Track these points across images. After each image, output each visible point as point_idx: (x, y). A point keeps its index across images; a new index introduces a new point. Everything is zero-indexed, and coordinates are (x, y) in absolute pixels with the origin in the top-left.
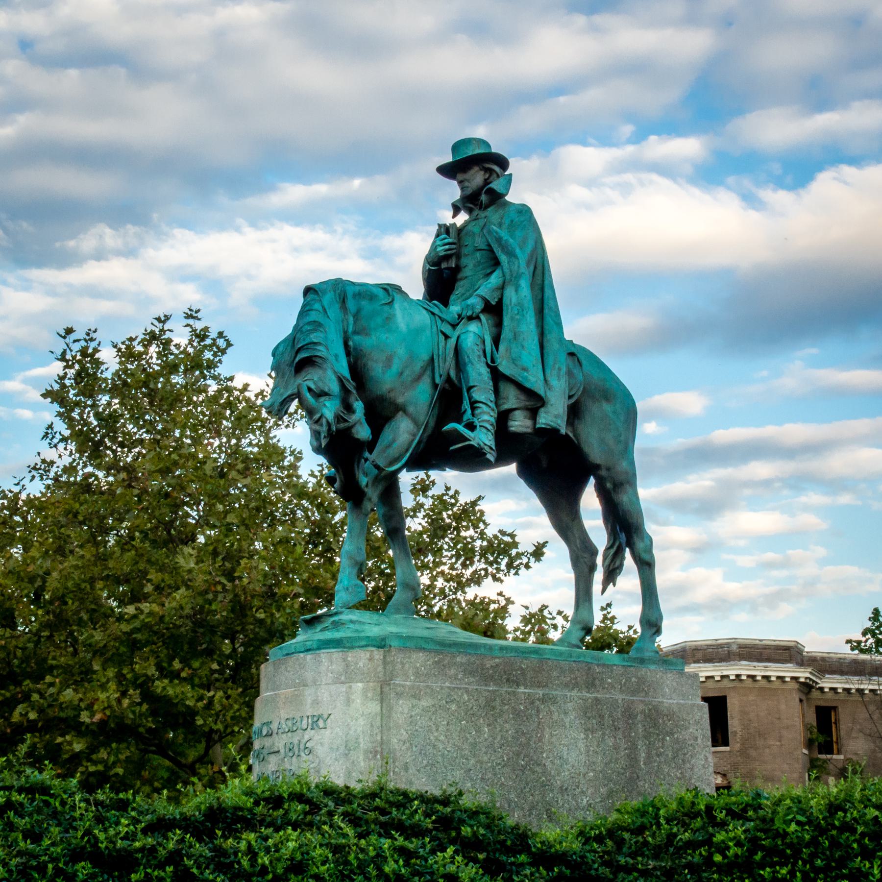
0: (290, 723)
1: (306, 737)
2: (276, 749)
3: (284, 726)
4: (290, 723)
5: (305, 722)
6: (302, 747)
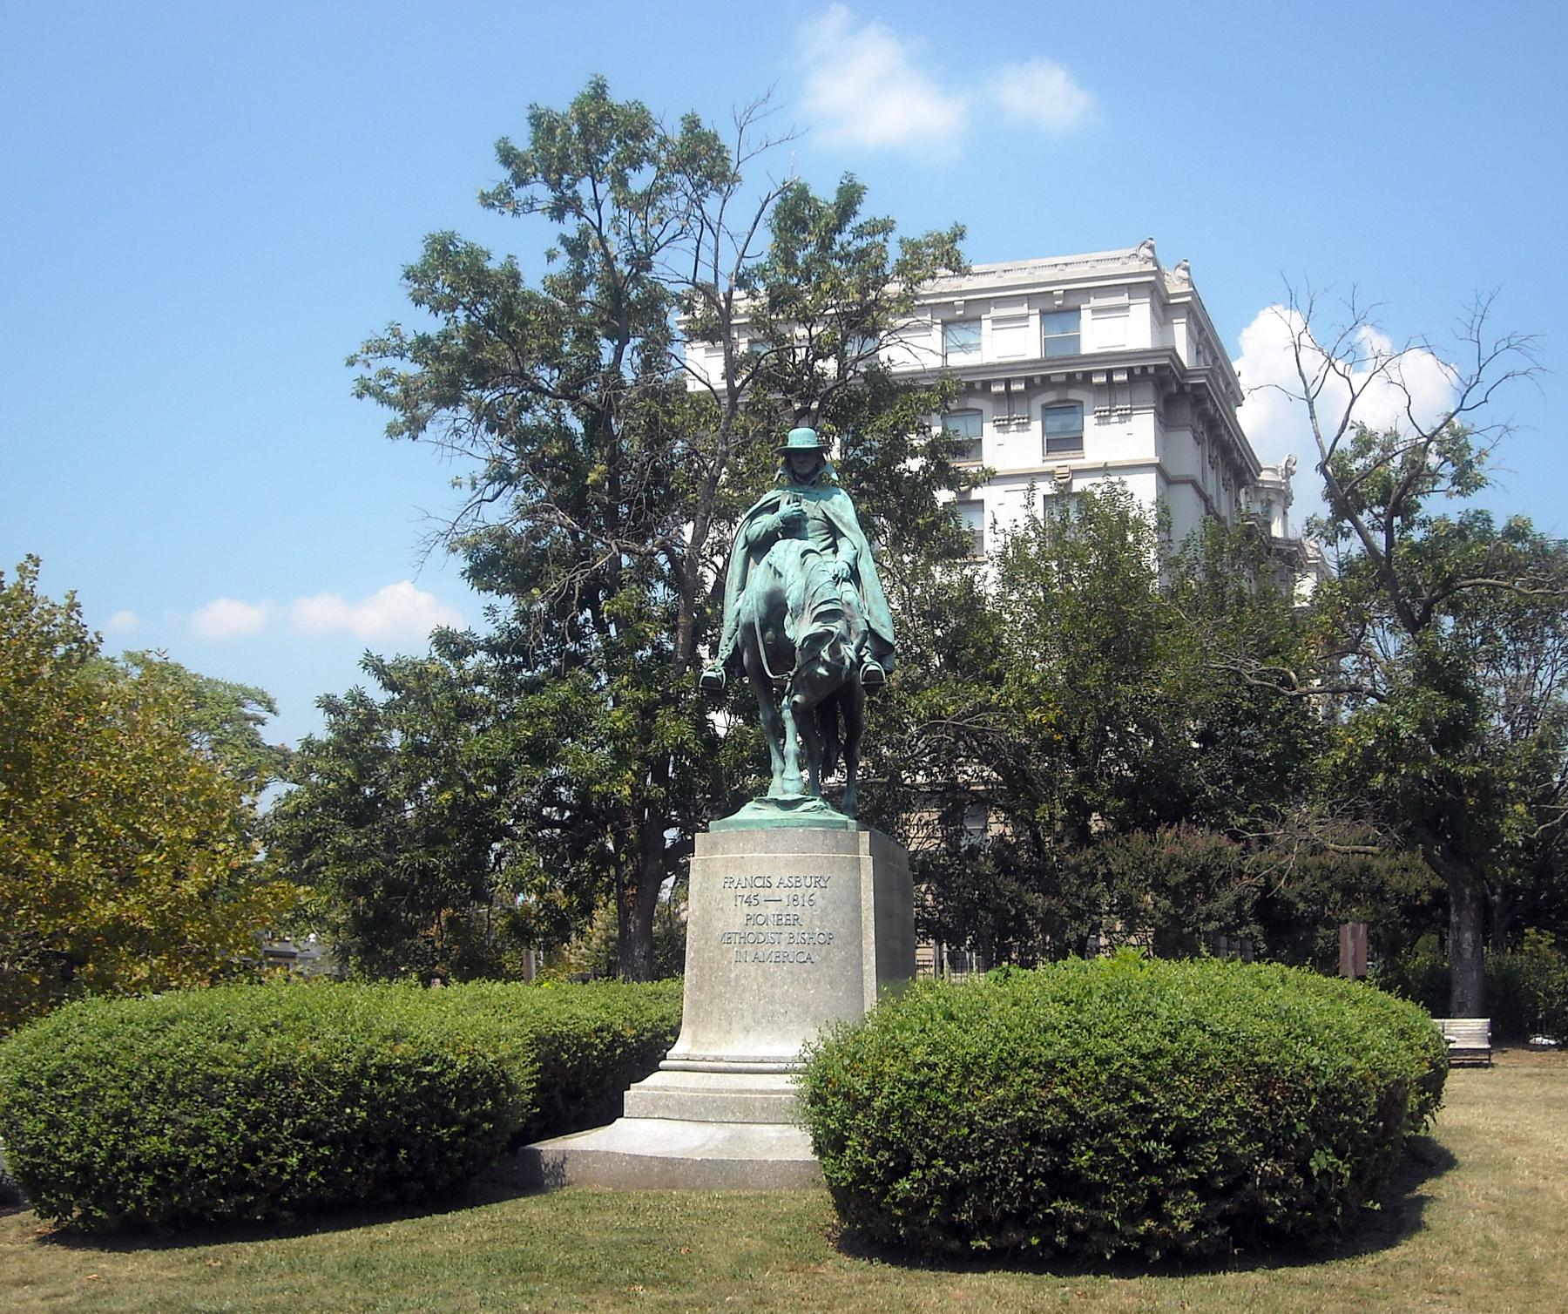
0: (793, 880)
1: (810, 892)
4: (793, 880)
6: (807, 899)
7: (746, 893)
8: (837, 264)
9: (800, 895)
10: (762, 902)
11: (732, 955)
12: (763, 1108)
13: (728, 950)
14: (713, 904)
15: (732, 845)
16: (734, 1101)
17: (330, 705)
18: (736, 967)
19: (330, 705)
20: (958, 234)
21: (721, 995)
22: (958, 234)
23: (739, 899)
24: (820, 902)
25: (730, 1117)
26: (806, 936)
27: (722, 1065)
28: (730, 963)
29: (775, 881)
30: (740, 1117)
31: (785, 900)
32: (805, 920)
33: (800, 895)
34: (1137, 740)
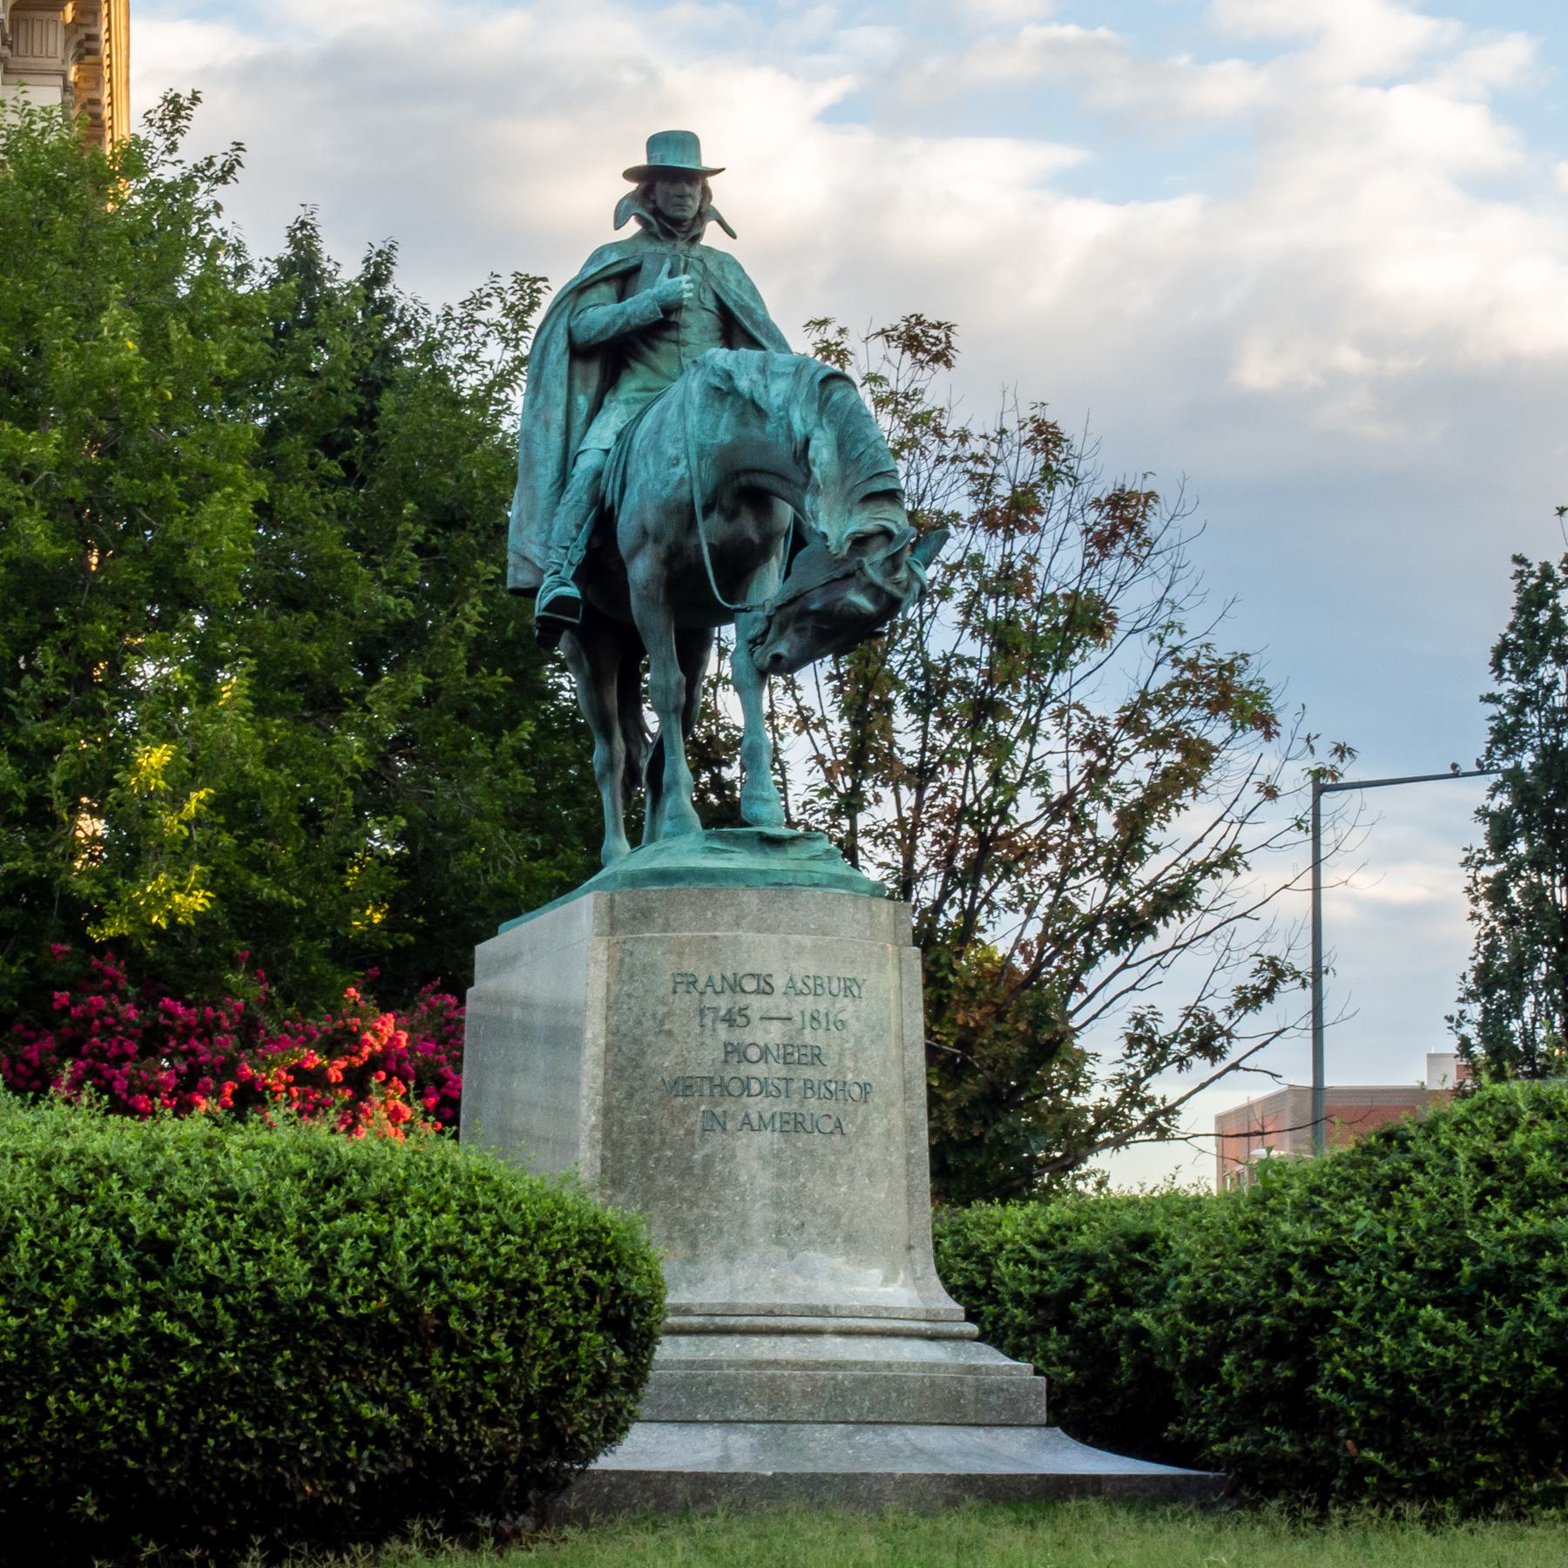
0: (811, 983)
2: (785, 1015)
3: (800, 985)
5: (835, 984)
7: (723, 1003)
8: (52, 266)
9: (823, 1011)
10: (755, 1022)
11: (695, 1119)
12: (804, 1394)
13: (685, 1110)
14: (648, 1023)
15: (688, 914)
16: (749, 1382)
17: (630, 174)
18: (704, 1141)
19: (630, 174)
20: (948, 364)
21: (670, 1193)
22: (948, 364)
23: (709, 1016)
24: (854, 1025)
25: (742, 1412)
26: (833, 1087)
27: (695, 1321)
28: (690, 1132)
29: (779, 982)
30: (761, 1410)
31: (798, 1019)
32: (831, 1059)
33: (823, 1011)
34: (1048, 1150)
